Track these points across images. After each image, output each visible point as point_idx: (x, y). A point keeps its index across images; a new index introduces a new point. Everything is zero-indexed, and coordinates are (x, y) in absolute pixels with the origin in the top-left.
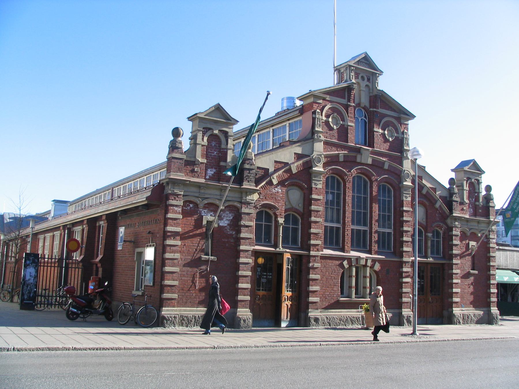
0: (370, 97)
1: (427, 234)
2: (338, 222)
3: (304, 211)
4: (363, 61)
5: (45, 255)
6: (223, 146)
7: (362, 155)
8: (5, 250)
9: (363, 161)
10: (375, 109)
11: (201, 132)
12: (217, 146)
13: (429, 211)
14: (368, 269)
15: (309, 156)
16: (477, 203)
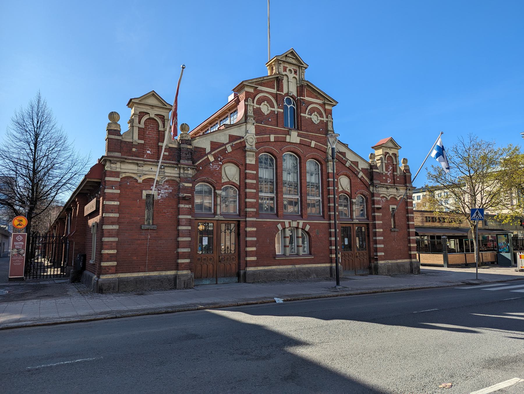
0: (297, 87)
1: (351, 200)
2: (272, 192)
3: (240, 184)
4: (290, 55)
5: (53, 234)
6: (161, 129)
7: (290, 135)
8: (287, 258)
9: (291, 141)
10: (301, 98)
11: (138, 116)
12: (148, 123)
13: (352, 181)
14: (300, 231)
15: (243, 138)
16: (395, 173)
